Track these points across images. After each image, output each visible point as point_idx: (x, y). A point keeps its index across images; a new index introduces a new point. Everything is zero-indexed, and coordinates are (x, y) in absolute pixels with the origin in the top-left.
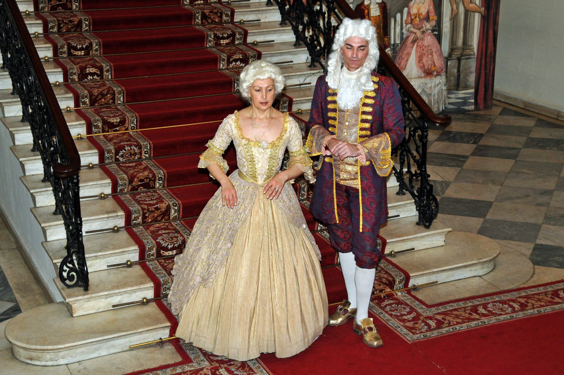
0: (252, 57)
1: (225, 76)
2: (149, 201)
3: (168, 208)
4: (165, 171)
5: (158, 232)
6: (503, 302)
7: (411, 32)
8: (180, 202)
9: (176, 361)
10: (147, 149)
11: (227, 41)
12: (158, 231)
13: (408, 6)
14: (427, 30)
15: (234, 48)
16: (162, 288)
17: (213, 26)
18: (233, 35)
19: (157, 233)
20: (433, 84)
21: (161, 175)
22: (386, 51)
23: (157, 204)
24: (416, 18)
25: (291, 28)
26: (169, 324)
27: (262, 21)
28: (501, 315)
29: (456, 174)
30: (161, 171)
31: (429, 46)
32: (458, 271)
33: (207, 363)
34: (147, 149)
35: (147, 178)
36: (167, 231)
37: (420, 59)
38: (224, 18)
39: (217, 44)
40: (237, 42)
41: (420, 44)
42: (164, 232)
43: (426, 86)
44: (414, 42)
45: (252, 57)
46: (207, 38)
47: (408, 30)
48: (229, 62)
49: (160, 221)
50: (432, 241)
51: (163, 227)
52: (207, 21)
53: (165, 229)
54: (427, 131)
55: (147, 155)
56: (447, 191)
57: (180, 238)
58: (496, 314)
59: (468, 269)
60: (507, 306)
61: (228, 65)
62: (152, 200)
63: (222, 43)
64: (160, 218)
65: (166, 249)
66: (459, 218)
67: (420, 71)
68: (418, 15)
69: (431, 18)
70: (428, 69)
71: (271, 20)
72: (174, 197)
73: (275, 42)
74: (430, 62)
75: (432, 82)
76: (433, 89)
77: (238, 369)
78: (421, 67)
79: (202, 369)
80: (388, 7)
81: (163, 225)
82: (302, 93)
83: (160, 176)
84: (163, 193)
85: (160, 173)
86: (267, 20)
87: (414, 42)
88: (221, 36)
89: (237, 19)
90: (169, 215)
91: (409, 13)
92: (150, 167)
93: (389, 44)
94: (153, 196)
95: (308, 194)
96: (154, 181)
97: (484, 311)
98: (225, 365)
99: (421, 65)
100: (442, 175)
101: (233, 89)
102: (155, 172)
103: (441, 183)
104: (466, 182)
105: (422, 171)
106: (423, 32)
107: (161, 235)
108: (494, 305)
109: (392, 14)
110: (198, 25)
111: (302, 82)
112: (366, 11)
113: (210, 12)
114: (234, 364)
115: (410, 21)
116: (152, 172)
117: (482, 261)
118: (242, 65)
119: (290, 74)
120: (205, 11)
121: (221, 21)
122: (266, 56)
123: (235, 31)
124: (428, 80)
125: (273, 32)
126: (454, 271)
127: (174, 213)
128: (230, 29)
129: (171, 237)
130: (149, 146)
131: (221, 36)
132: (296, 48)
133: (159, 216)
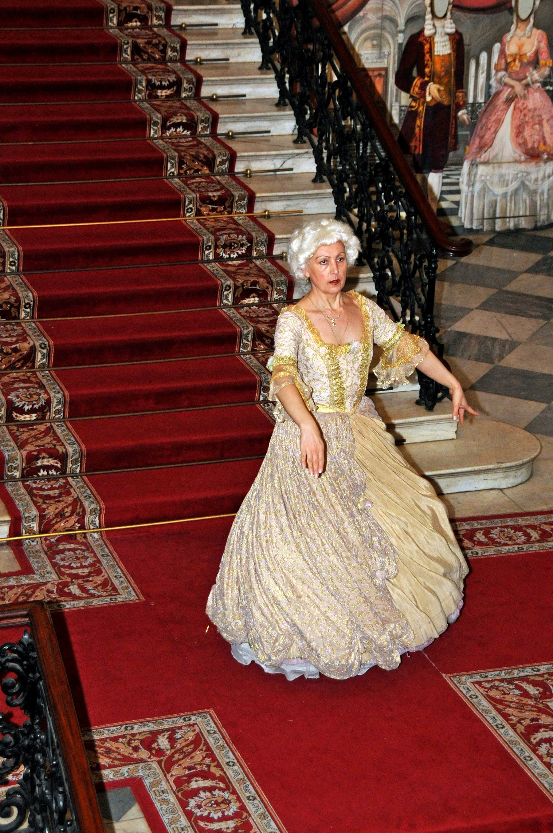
0: (202, 121)
1: (154, 149)
2: (6, 337)
3: (33, 350)
4: (36, 294)
5: (13, 384)
6: (517, 528)
7: (506, 85)
8: (52, 342)
9: (12, 570)
10: (14, 258)
11: (169, 92)
12: (13, 383)
13: (500, 41)
14: (533, 83)
15: (178, 104)
16: (6, 467)
17: (149, 65)
18: (178, 83)
19: (10, 387)
20: (541, 175)
21: (29, 299)
22: (460, 113)
23: (16, 342)
24: (514, 60)
25: (273, 76)
26: (8, 518)
27: (231, 61)
28: (506, 545)
29: (535, 330)
30: (30, 294)
31: (535, 109)
32: (465, 478)
33: (54, 576)
34: (14, 258)
35: (7, 303)
36: (26, 385)
37: (519, 131)
38: (169, 53)
39: (152, 96)
40: (184, 95)
41: (520, 105)
42: (22, 385)
43: (528, 177)
44: (509, 101)
45: (202, 121)
46: (136, 86)
47: (500, 81)
48: (165, 128)
49: (19, 368)
50: (436, 431)
51: (22, 378)
52: (141, 57)
53: (24, 381)
54: (435, 263)
55: (14, 268)
56: (508, 357)
57: (44, 396)
58: (500, 543)
59: (482, 477)
60: (520, 534)
61: (163, 132)
62: (10, 336)
63: (159, 94)
64: (19, 365)
65: (21, 411)
66: (508, 400)
67: (519, 151)
68: (519, 56)
69: (542, 62)
70: (533, 148)
71: (248, 60)
72: (45, 334)
73: (247, 97)
74: (536, 137)
75: (538, 171)
76: (540, 182)
77: (96, 587)
78: (520, 145)
79: (45, 584)
80: (466, 41)
81: (23, 376)
82: (277, 184)
83: (27, 301)
84: (30, 327)
85: (28, 296)
86: (240, 60)
87: (509, 101)
88: (158, 83)
89: (190, 55)
90: (34, 362)
91: (502, 52)
92: (15, 285)
93: (465, 103)
94: (15, 330)
95: (254, 345)
96: (18, 308)
97: (483, 538)
98: (80, 581)
99: (521, 141)
100: (510, 330)
101: (164, 172)
102: (20, 295)
103: (503, 343)
104: (545, 345)
105: (427, 322)
106: (527, 86)
107: (16, 389)
108: (501, 531)
109: (472, 53)
110: (126, 61)
111: (278, 166)
112: (427, 46)
113: (146, 43)
114: (92, 581)
115: (503, 67)
116: (16, 294)
117: (504, 465)
118: (185, 132)
119: (259, 153)
120: (139, 41)
121: (164, 58)
122: (227, 120)
123: (182, 76)
124: (531, 167)
125: (244, 82)
126: (458, 478)
127: (42, 359)
128: (175, 73)
129: (30, 394)
130: (16, 253)
131: (158, 83)
132: (279, 110)
133: (19, 361)
